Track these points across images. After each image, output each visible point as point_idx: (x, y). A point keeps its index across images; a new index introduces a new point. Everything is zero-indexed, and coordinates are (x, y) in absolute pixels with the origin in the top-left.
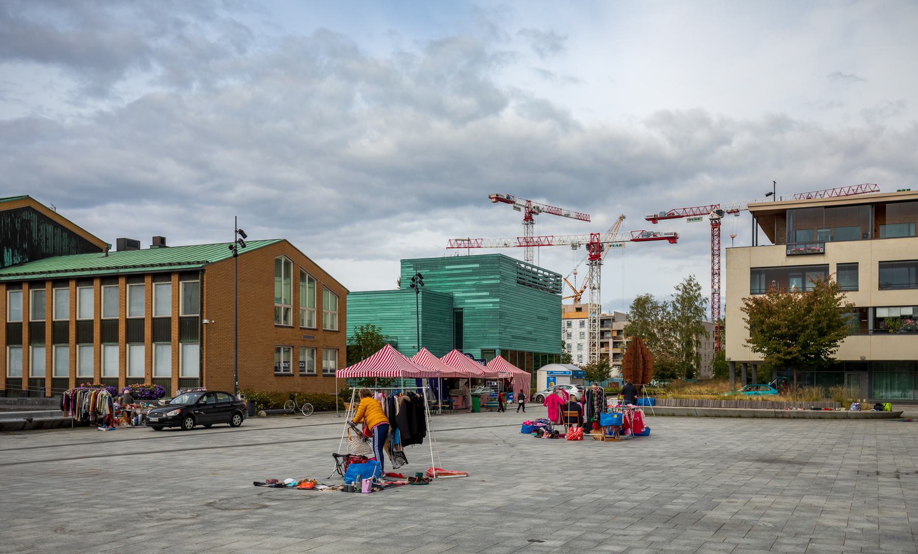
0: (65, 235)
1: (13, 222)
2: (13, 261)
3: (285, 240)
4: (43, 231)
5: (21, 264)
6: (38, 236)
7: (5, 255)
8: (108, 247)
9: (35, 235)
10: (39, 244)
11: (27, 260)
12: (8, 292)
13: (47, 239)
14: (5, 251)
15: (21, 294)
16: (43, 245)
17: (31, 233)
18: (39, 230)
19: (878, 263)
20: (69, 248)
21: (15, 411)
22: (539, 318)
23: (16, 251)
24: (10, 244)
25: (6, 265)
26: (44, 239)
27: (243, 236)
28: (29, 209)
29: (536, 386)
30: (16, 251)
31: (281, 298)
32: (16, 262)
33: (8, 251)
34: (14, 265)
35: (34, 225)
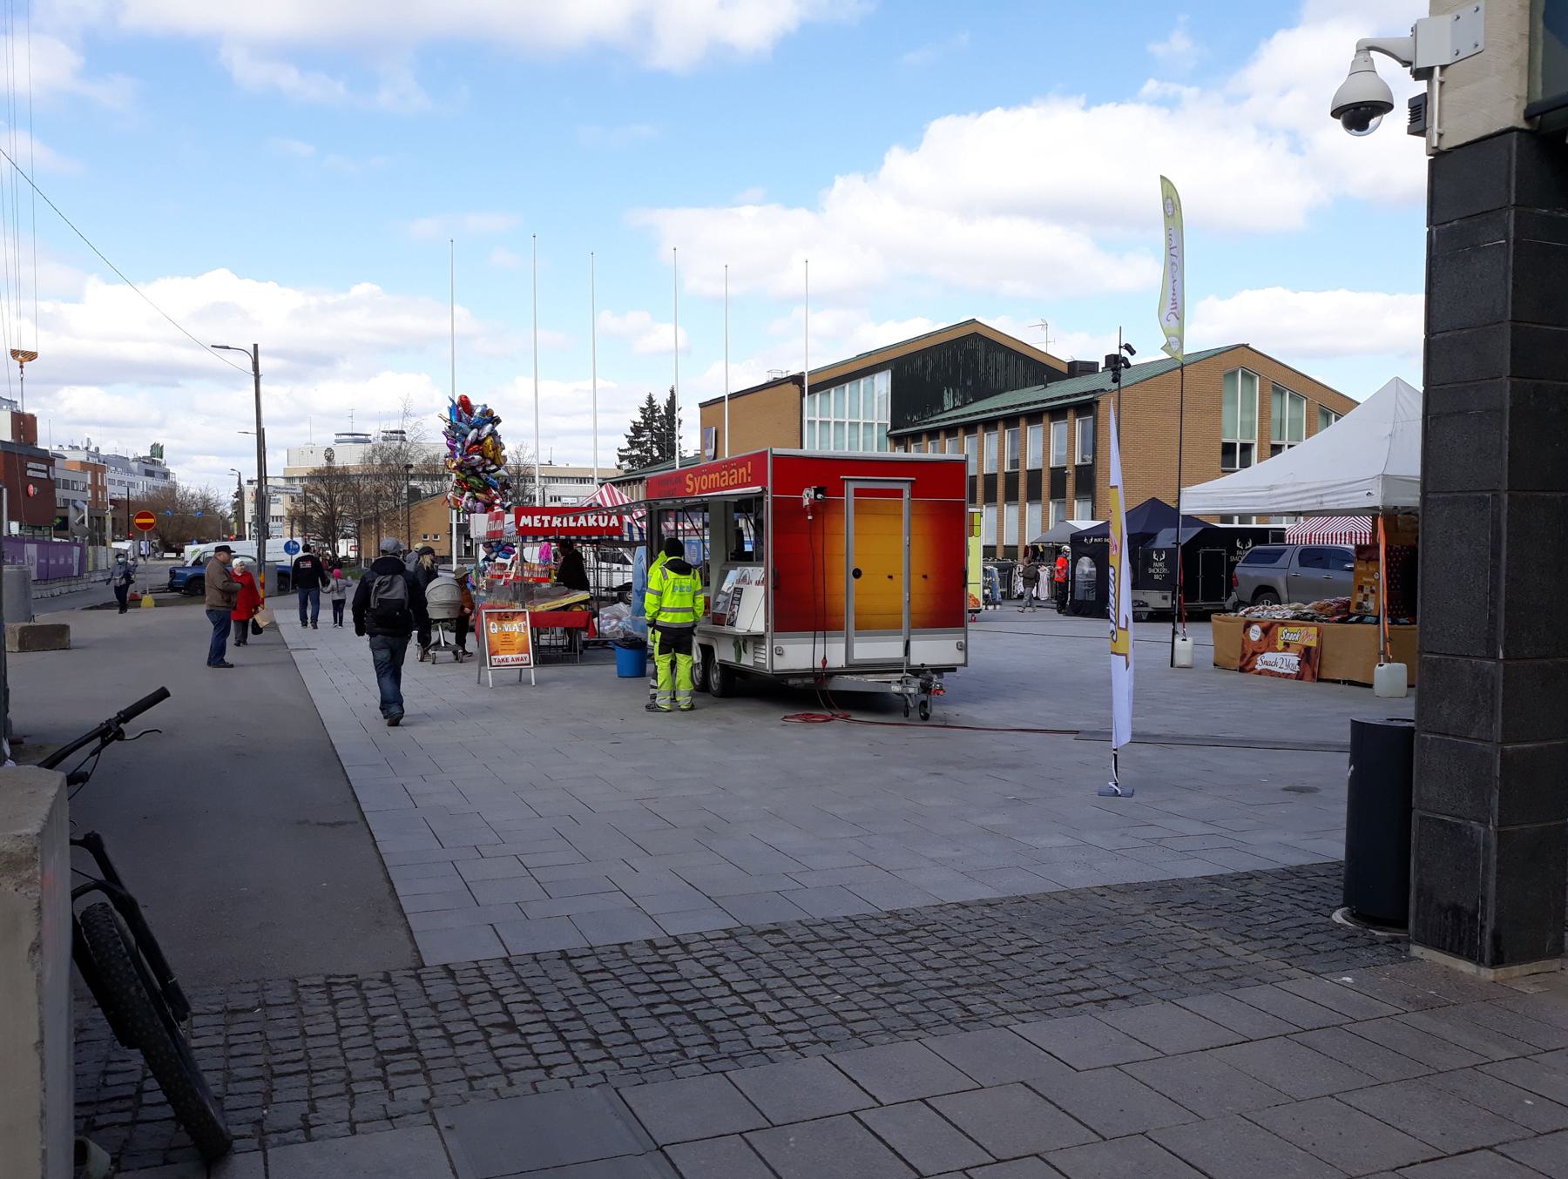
0: (1021, 363)
1: (955, 355)
2: (954, 403)
3: (1246, 346)
4: (991, 362)
5: (965, 404)
6: (985, 368)
7: (946, 397)
8: (1096, 364)
9: (981, 368)
10: (987, 379)
11: (971, 400)
12: (947, 440)
13: (996, 370)
14: (946, 391)
15: (997, 436)
16: (992, 379)
17: (977, 365)
18: (987, 361)
19: (698, 410)
20: (1026, 379)
21: (149, 977)
22: (1502, 322)
23: (958, 390)
24: (952, 383)
25: (945, 409)
26: (992, 371)
27: (1130, 352)
28: (976, 337)
29: (1043, 517)
30: (958, 390)
31: (451, 557)
32: (958, 403)
33: (948, 392)
34: (955, 408)
35: (981, 356)
